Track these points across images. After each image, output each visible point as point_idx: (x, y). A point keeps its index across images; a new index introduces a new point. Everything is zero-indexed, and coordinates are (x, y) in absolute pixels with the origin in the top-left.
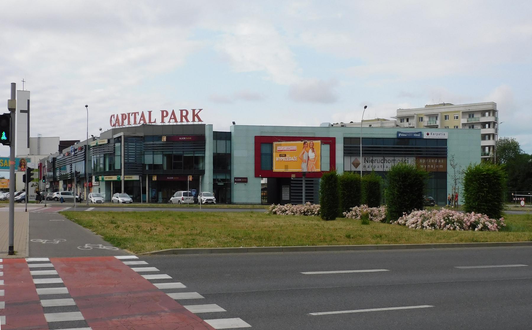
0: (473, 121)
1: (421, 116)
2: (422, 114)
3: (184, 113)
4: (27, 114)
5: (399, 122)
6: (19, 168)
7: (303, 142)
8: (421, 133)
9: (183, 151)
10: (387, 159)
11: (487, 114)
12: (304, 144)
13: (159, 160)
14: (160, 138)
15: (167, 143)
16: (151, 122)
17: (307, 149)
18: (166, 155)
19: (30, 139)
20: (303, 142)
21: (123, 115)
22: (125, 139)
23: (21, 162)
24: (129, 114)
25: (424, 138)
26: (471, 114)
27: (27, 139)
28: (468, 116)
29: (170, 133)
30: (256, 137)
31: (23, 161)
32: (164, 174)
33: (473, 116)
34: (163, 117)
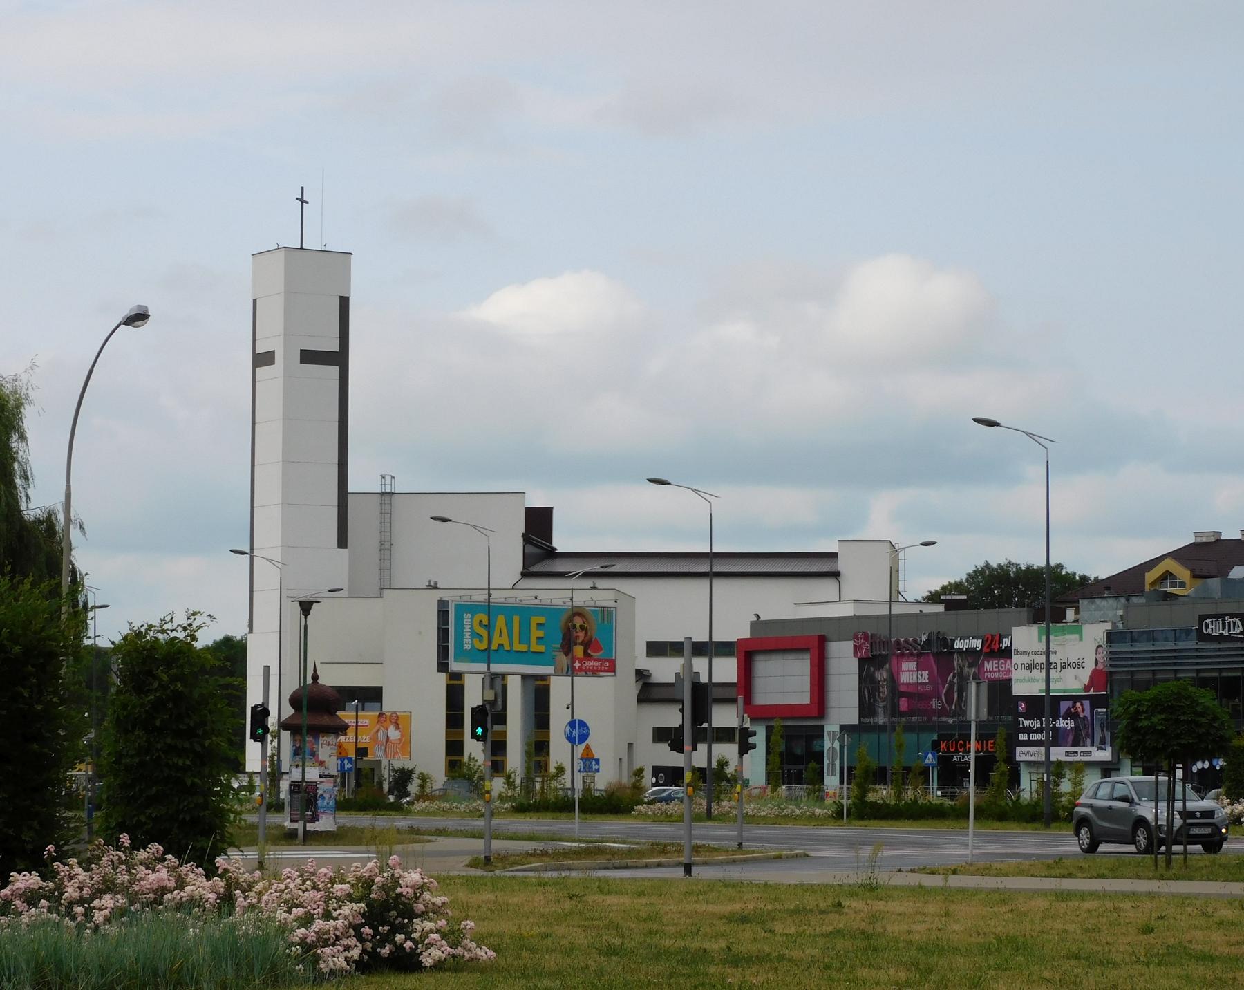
4: (334, 370)
6: (563, 659)
9: (1153, 670)
15: (1063, 606)
16: (552, 554)
17: (385, 724)
23: (569, 629)
31: (578, 621)
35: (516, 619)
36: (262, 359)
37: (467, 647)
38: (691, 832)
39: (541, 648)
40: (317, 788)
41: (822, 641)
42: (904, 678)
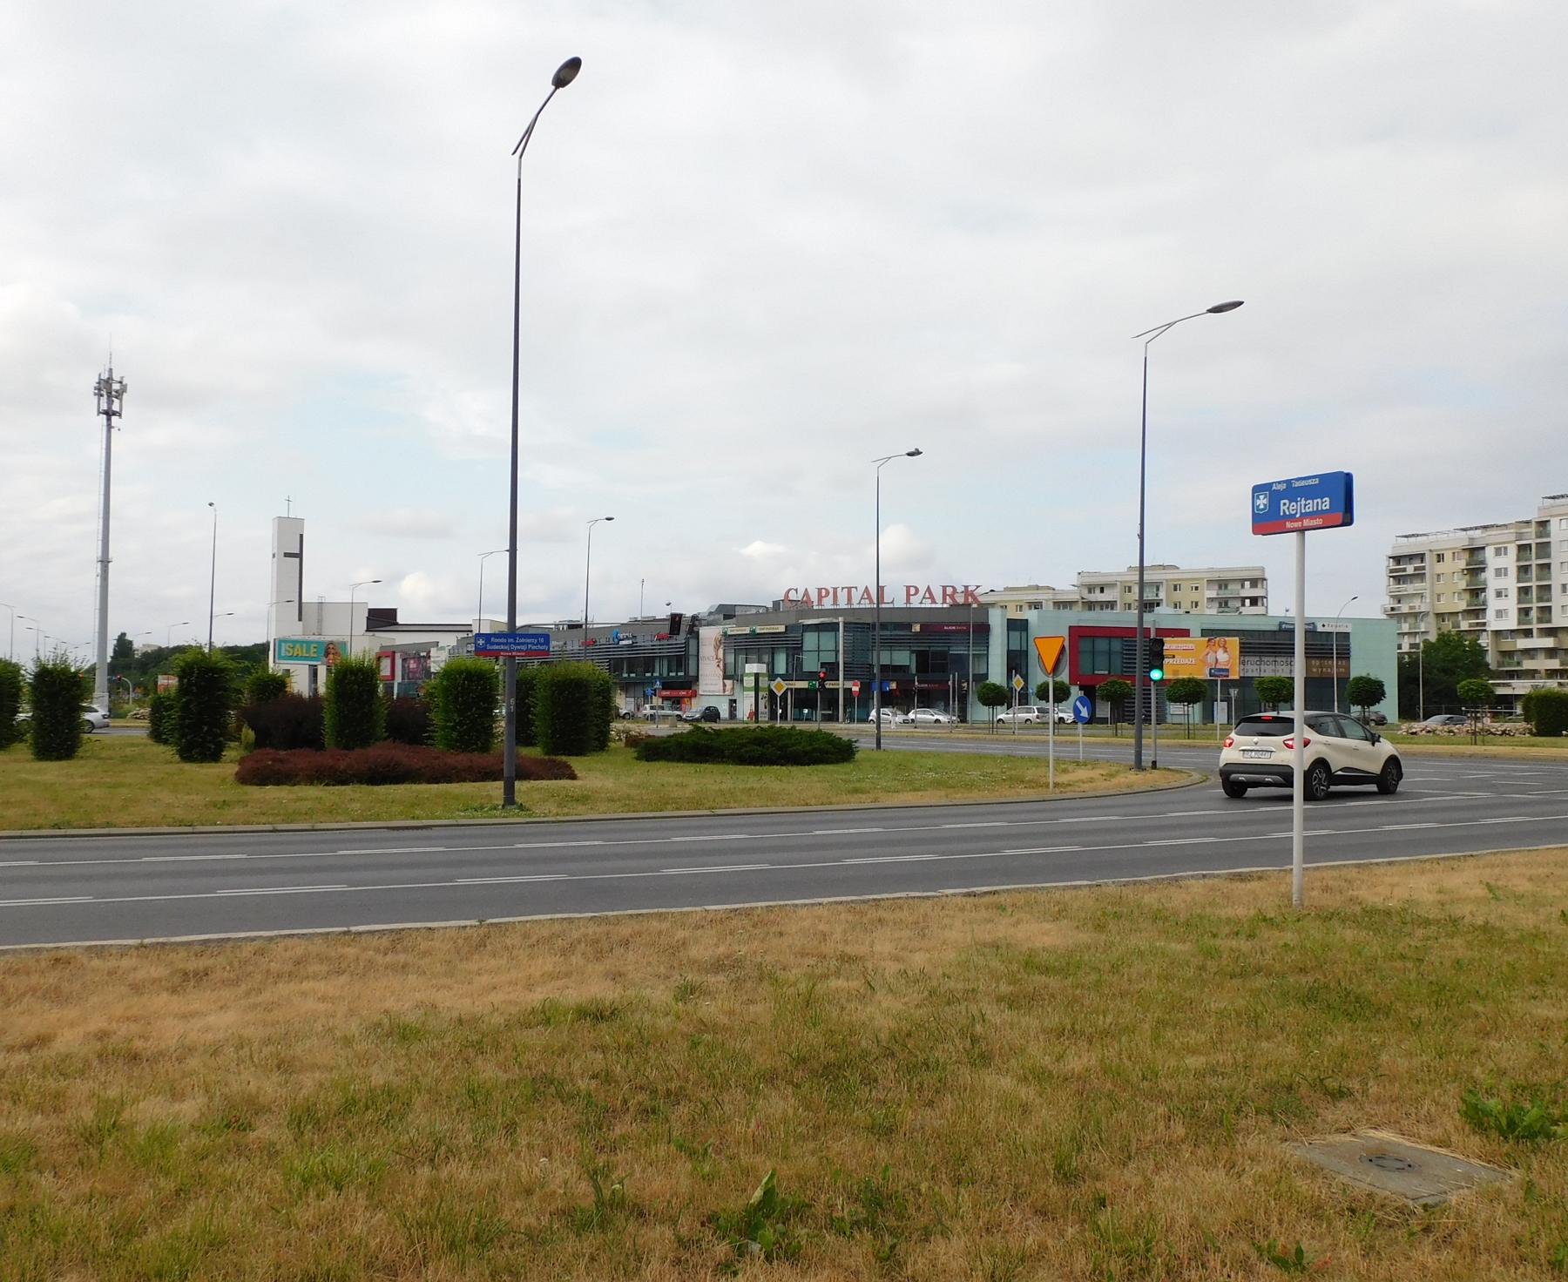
0: (1224, 594)
1: (1129, 584)
2: (1131, 582)
3: (949, 590)
4: (298, 560)
5: (1085, 593)
7: (1207, 639)
8: (1313, 623)
10: (1278, 659)
11: (1247, 584)
12: (1209, 640)
13: (903, 658)
14: (909, 626)
18: (913, 652)
19: (303, 605)
20: (1207, 639)
21: (820, 590)
22: (844, 627)
24: (835, 589)
25: (1319, 630)
26: (1222, 584)
27: (109, 598)
28: (1217, 587)
29: (926, 620)
30: (1070, 627)
31: (331, 646)
32: (1153, 688)
33: (1226, 587)
34: (908, 595)
35: (304, 645)
36: (274, 556)
37: (283, 655)
38: (1141, 732)
39: (315, 655)
40: (336, 703)
41: (394, 653)
42: (411, 666)
